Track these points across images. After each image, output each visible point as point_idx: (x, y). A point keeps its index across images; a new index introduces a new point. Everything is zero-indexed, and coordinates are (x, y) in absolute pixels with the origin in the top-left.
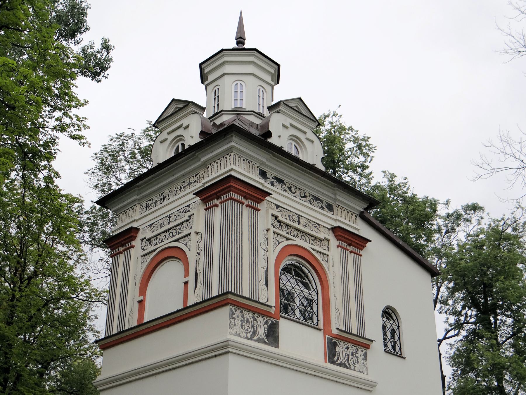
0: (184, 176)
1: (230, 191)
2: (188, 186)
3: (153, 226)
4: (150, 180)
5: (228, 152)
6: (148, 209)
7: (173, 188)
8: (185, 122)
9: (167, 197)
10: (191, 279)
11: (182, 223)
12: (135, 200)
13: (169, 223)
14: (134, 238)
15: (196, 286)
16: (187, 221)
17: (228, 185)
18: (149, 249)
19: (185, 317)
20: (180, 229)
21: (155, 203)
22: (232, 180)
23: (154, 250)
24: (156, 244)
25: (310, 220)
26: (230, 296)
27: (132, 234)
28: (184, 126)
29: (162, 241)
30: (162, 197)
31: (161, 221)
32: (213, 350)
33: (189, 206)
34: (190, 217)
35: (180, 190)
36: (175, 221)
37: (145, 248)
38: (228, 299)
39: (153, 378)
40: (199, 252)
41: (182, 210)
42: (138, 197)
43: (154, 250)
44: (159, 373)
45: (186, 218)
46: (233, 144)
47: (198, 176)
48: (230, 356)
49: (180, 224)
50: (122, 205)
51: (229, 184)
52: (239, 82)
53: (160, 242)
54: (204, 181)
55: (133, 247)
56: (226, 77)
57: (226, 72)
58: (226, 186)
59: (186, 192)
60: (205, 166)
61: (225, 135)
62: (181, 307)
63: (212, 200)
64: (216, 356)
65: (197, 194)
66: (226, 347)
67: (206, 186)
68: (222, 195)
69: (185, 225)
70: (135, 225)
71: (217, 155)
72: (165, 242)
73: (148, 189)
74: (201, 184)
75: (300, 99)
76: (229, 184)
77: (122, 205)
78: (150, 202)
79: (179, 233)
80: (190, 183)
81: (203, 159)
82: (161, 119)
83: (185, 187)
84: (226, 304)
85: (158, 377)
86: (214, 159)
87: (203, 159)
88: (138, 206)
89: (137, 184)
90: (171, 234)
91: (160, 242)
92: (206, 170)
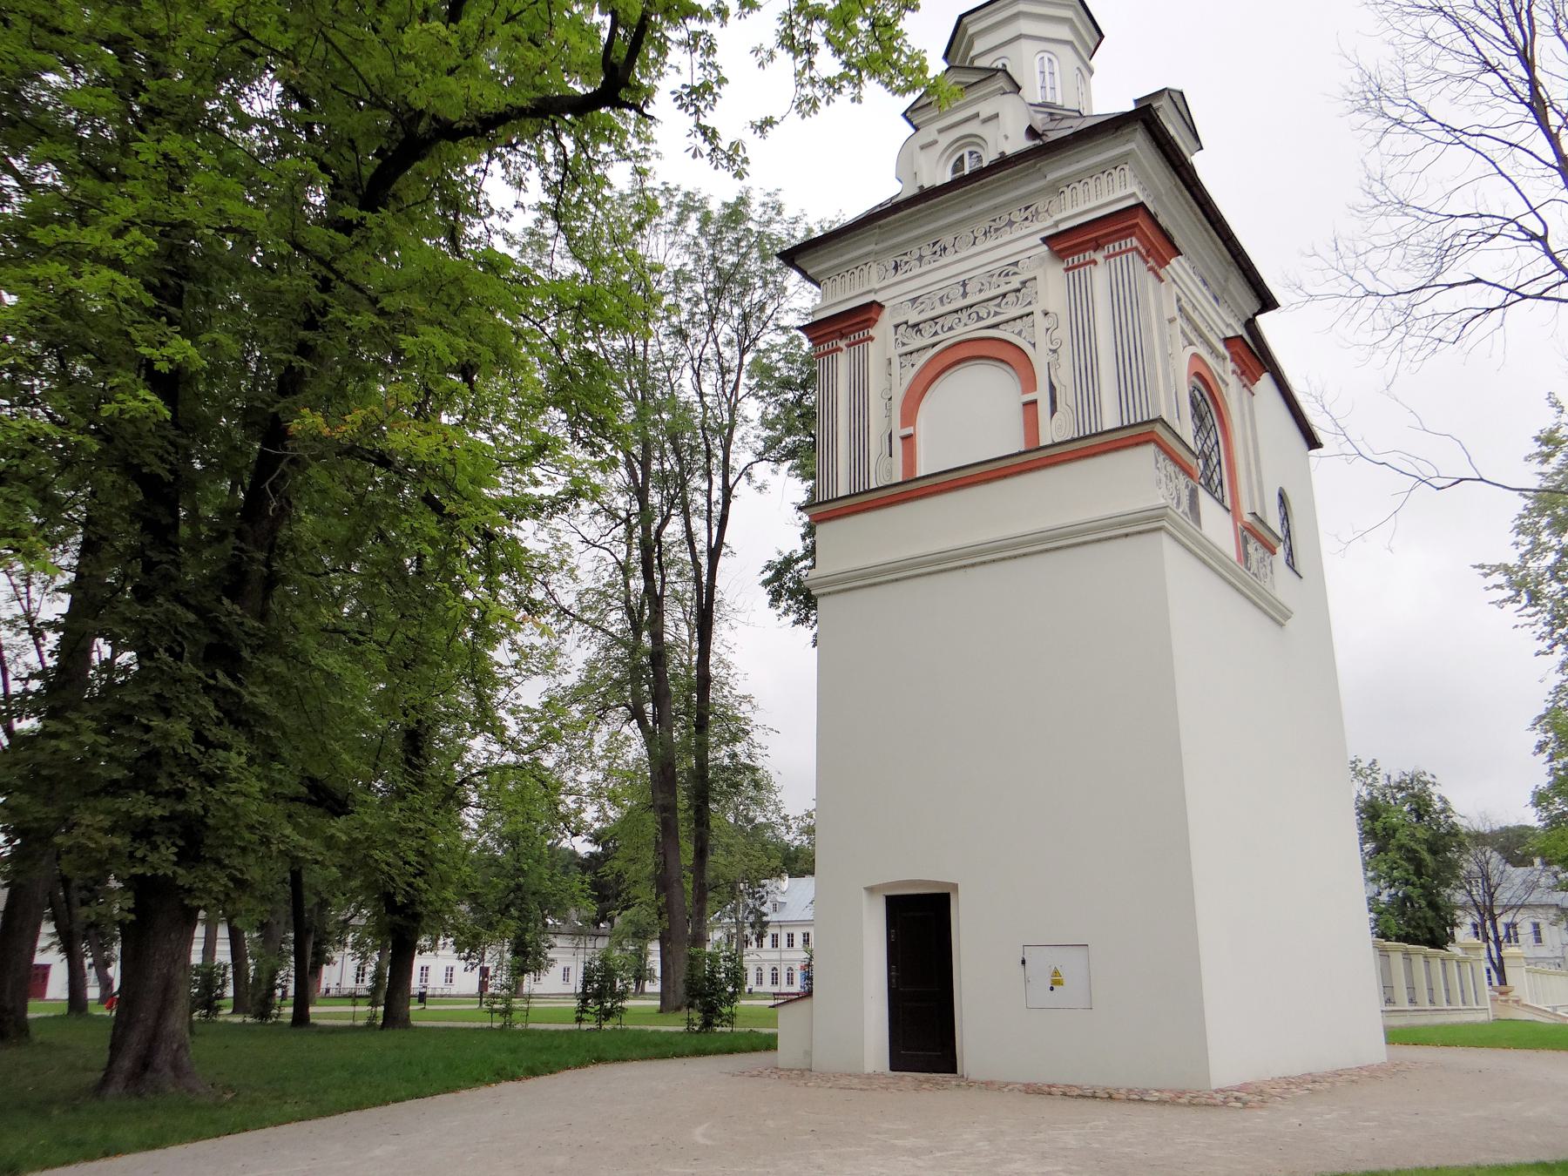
0: (995, 208)
1: (1130, 235)
2: (1008, 228)
3: (920, 300)
4: (912, 214)
5: (1116, 164)
6: (899, 272)
7: (965, 231)
8: (986, 109)
9: (950, 250)
10: (1042, 395)
11: (1004, 295)
12: (867, 254)
13: (965, 295)
14: (871, 322)
15: (1054, 410)
16: (1018, 290)
17: (1130, 223)
18: (917, 342)
19: (1097, 450)
20: (999, 305)
21: (921, 258)
22: (1141, 212)
23: (934, 345)
24: (936, 333)
25: (1196, 329)
26: (1158, 428)
27: (873, 315)
28: (983, 116)
29: (951, 329)
30: (937, 248)
31: (941, 293)
32: (1122, 525)
33: (1016, 264)
34: (1024, 283)
35: (985, 234)
36: (981, 291)
37: (905, 341)
38: (1152, 432)
39: (961, 573)
40: (1054, 348)
41: (998, 271)
42: (877, 248)
43: (934, 345)
44: (973, 565)
45: (1015, 284)
46: (1132, 146)
47: (1033, 208)
48: (1163, 536)
49: (997, 297)
50: (836, 262)
51: (1135, 221)
52: (1046, 56)
53: (945, 329)
54: (1058, 217)
55: (871, 339)
56: (1023, 42)
57: (1024, 32)
58: (1125, 224)
59: (1000, 241)
60: (1055, 189)
61: (1117, 129)
62: (1019, 446)
63: (1085, 251)
64: (1127, 535)
65: (1046, 240)
66: (1159, 518)
67: (1063, 227)
68: (1109, 242)
69: (1011, 298)
70: (879, 298)
71: (1088, 169)
72: (960, 330)
73: (902, 233)
74: (1050, 222)
75: (1182, 93)
76: (1135, 221)
77: (836, 262)
78: (906, 258)
79: (996, 314)
80: (1011, 223)
81: (1051, 177)
82: (918, 105)
83: (997, 230)
84: (1147, 442)
85: (970, 571)
86: (1079, 177)
87: (1051, 177)
88: (874, 266)
89: (881, 222)
90: (974, 316)
91: (945, 329)
92: (1055, 198)
